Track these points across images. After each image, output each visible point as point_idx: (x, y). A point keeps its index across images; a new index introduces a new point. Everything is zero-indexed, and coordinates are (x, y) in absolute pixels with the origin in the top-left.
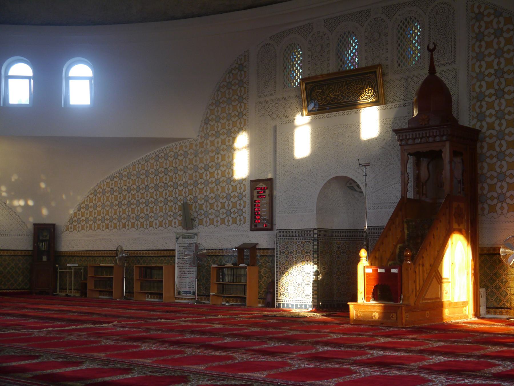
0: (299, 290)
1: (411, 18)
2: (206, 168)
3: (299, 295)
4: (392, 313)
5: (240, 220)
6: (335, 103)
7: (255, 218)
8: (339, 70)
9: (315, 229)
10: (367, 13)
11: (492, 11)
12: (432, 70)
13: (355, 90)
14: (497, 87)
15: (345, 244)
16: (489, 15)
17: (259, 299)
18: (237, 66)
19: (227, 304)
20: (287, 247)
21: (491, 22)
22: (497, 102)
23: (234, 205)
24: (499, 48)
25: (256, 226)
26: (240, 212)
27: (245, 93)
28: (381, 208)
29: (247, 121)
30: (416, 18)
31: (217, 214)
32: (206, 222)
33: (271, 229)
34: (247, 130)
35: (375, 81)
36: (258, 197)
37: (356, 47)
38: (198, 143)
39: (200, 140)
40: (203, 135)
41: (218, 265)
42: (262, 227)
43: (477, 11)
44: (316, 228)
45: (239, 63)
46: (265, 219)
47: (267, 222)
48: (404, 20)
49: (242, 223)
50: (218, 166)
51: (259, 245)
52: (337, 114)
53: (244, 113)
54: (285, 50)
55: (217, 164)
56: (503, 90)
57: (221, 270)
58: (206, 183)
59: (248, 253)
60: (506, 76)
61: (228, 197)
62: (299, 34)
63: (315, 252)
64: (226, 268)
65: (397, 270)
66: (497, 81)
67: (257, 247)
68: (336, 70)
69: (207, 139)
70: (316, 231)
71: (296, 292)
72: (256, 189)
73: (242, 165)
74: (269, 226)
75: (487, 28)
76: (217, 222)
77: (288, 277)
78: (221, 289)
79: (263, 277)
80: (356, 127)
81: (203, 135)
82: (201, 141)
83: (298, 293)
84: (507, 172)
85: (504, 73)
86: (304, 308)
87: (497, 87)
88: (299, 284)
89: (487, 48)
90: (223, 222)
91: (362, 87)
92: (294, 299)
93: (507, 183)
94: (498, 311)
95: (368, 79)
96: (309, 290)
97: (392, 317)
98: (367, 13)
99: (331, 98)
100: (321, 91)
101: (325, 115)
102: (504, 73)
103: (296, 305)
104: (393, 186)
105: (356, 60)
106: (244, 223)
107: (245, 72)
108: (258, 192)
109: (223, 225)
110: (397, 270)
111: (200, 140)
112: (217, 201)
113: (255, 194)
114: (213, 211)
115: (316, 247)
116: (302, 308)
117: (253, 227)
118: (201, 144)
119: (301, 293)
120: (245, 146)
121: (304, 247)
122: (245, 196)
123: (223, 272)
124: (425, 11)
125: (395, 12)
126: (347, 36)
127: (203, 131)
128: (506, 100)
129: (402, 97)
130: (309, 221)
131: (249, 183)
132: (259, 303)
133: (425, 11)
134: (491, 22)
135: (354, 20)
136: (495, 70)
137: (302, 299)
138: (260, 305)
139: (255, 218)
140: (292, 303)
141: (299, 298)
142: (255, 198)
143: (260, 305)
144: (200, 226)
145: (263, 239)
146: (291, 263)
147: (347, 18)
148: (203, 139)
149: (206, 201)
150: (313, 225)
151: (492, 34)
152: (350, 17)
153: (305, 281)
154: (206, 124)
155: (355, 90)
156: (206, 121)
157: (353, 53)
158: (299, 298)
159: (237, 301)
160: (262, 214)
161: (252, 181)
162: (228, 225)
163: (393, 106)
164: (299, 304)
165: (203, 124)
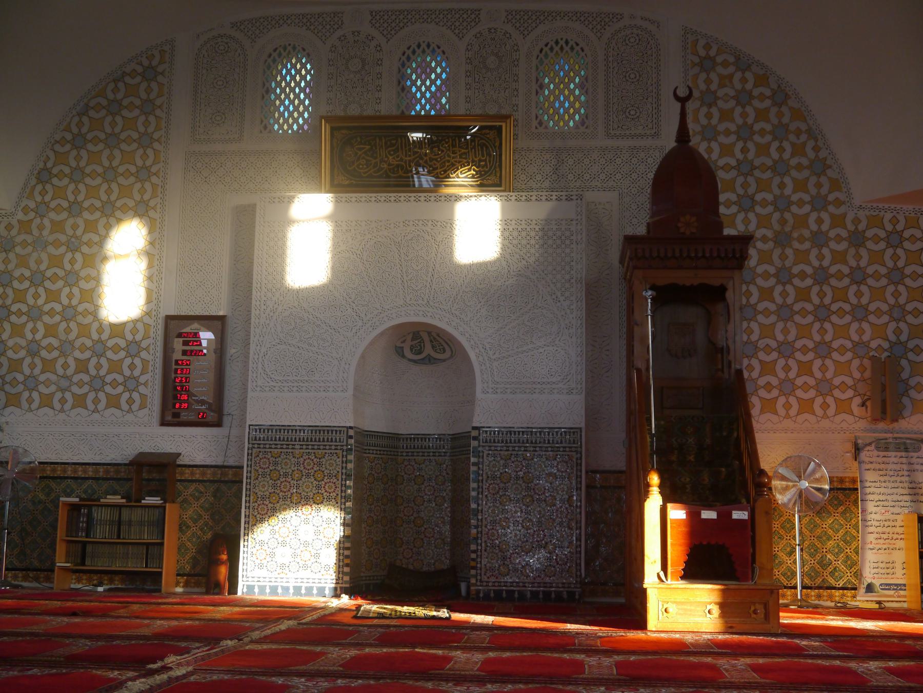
0: (306, 555)
1: (567, 42)
2: (37, 279)
3: (305, 567)
4: (754, 603)
5: (130, 402)
6: (400, 177)
7: (175, 397)
8: (403, 112)
9: (351, 428)
10: (473, 16)
11: (732, 59)
12: (683, 135)
13: (449, 156)
14: (741, 191)
15: (380, 462)
16: (725, 64)
17: (178, 575)
18: (140, 69)
19: (100, 589)
20: (276, 464)
21: (731, 77)
22: (741, 216)
23: (82, 366)
24: (745, 123)
25: (177, 415)
26: (131, 383)
27: (158, 128)
28: (513, 393)
29: (160, 189)
30: (577, 45)
31: (64, 383)
32: (30, 401)
33: (218, 424)
34: (141, 211)
35: (497, 144)
36: (184, 353)
37: (444, 76)
38: (14, 222)
39: (20, 216)
40: (32, 205)
41: (81, 499)
42: (192, 417)
43: (702, 53)
44: (352, 425)
45: (146, 63)
46: (203, 402)
47: (210, 409)
48: (553, 43)
49: (135, 407)
50: (72, 278)
51: (181, 457)
52: (393, 199)
53: (154, 169)
54: (270, 55)
55: (68, 273)
56: (752, 198)
57: (84, 511)
58: (35, 314)
59: (153, 474)
60: (757, 173)
61: (65, 348)
62: (308, 29)
63: (348, 476)
64: (102, 506)
65: (746, 513)
66: (740, 180)
67: (179, 462)
68: (395, 112)
69: (42, 216)
70: (351, 433)
71: (298, 560)
72: (180, 335)
73: (124, 279)
74: (212, 416)
75: (721, 86)
76: (63, 401)
77: (276, 528)
78: (80, 553)
79: (188, 527)
80: (443, 229)
81: (32, 205)
82: (26, 218)
83: (302, 563)
84: (760, 342)
85: (754, 167)
86: (318, 595)
87: (741, 191)
88: (306, 544)
89: (721, 120)
90: (80, 401)
91: (465, 153)
92: (290, 575)
93: (760, 361)
94: (31, 575)
95: (482, 139)
96: (330, 557)
97: (755, 612)
98: (473, 16)
99: (389, 165)
100: (368, 147)
101: (382, 196)
102: (754, 167)
103: (294, 587)
104: (541, 350)
105: (444, 100)
106: (142, 406)
107: (161, 85)
108: (185, 343)
109: (80, 410)
110: (746, 513)
111: (20, 216)
112: (63, 354)
113: (178, 345)
114: (53, 378)
115: (350, 466)
116: (312, 595)
117: (169, 418)
118: (25, 226)
119: (309, 563)
120: (296, 225)
121: (320, 464)
122: (147, 349)
123: (89, 515)
124: (599, 34)
125: (534, 25)
126: (424, 52)
127: (31, 196)
128: (757, 215)
129: (547, 184)
130: (336, 409)
131: (161, 323)
132: (177, 584)
133: (599, 34)
134: (731, 77)
135: (441, 24)
136: (738, 160)
137: (313, 576)
138: (179, 590)
139: (175, 397)
140: (285, 585)
141: (263, 573)
142: (177, 356)
143: (179, 590)
144: (12, 409)
145: (194, 446)
146: (285, 499)
147: (425, 16)
148: (32, 215)
149: (33, 354)
150: (344, 418)
151: (732, 97)
152: (433, 17)
153: (321, 537)
154: (39, 180)
155: (449, 156)
156: (43, 176)
157: (284, 105)
158: (263, 573)
159: (111, 581)
160: (194, 390)
161: (169, 318)
162: (96, 411)
163: (524, 198)
164: (304, 585)
165: (33, 182)
